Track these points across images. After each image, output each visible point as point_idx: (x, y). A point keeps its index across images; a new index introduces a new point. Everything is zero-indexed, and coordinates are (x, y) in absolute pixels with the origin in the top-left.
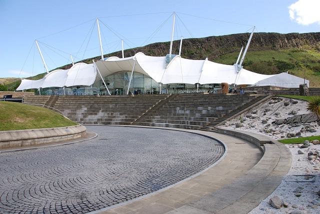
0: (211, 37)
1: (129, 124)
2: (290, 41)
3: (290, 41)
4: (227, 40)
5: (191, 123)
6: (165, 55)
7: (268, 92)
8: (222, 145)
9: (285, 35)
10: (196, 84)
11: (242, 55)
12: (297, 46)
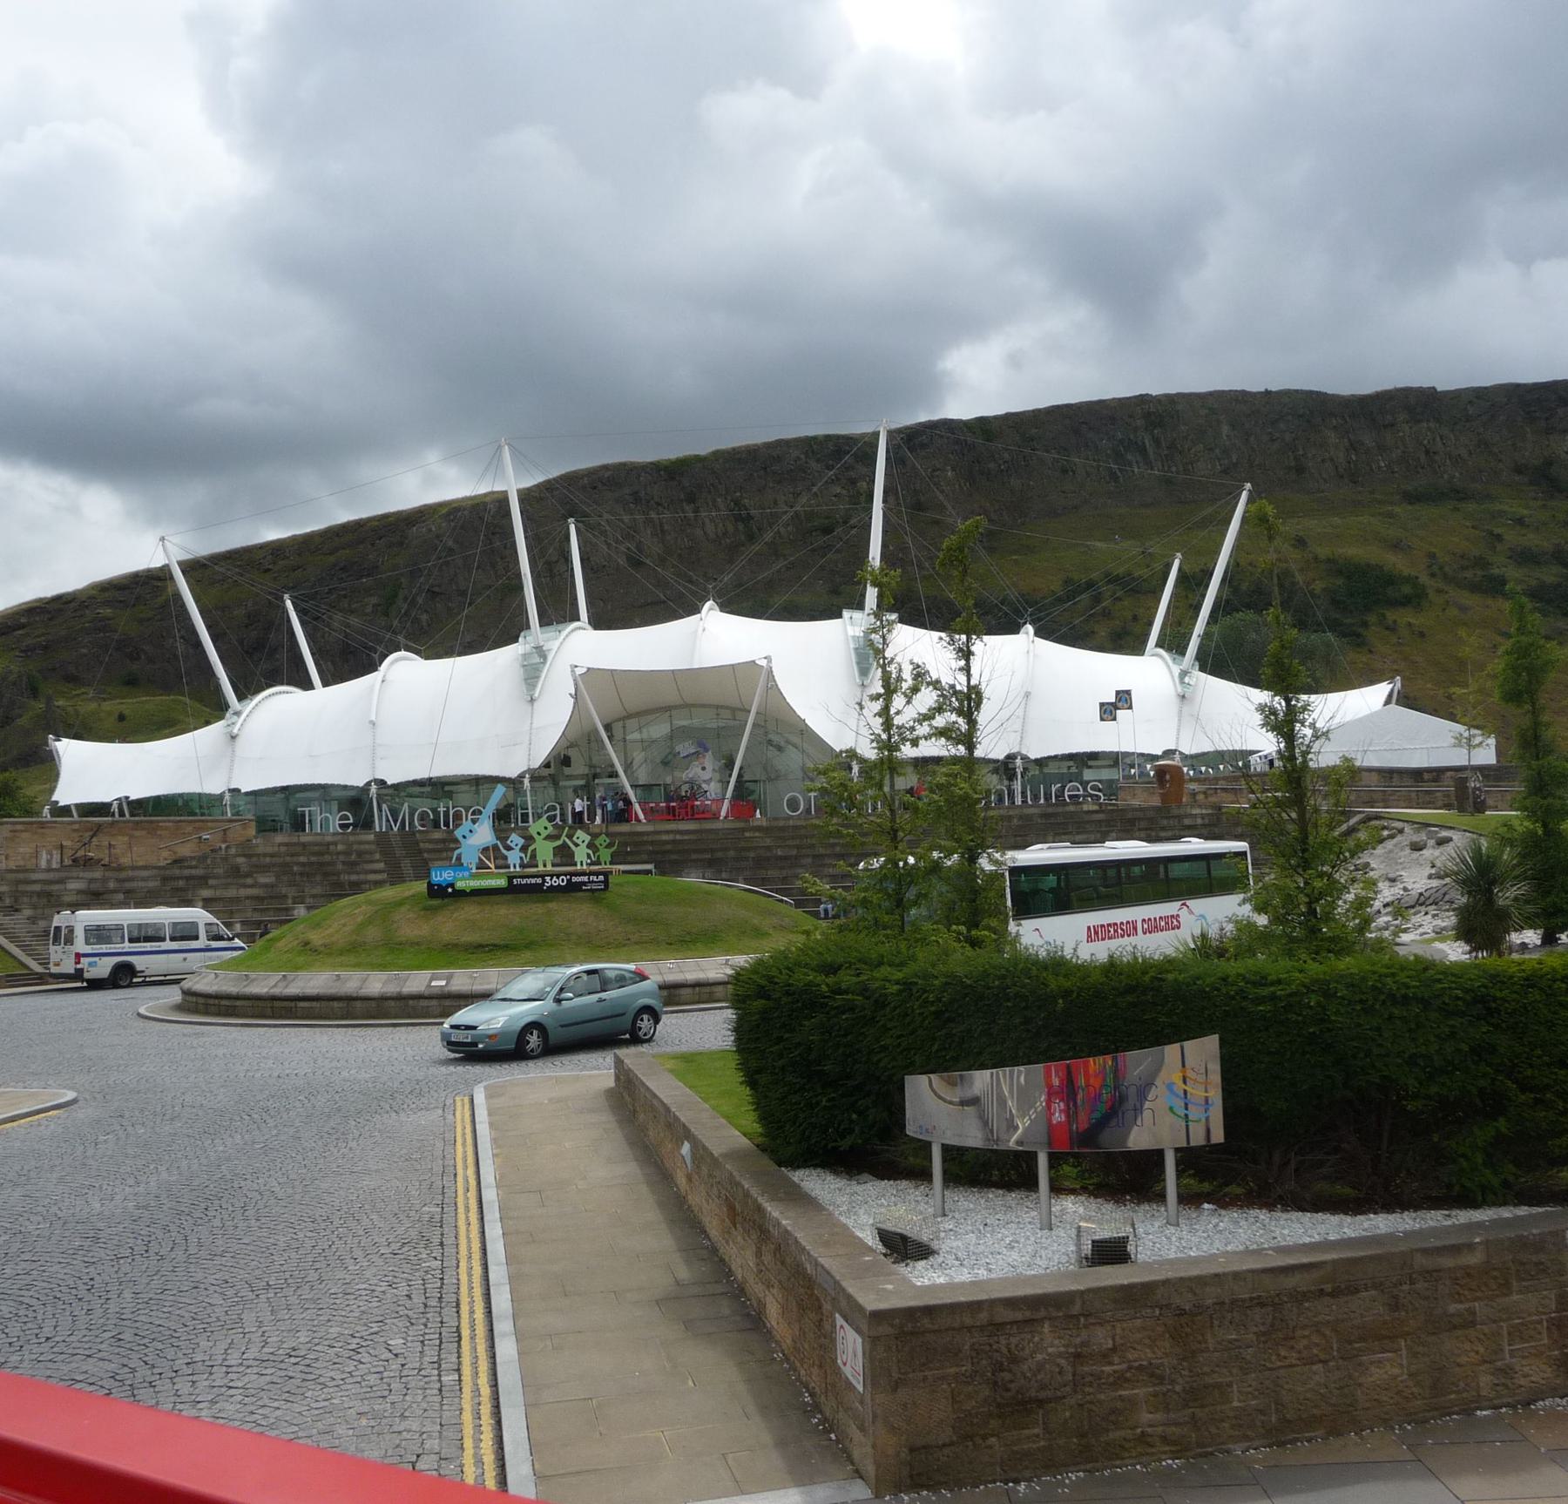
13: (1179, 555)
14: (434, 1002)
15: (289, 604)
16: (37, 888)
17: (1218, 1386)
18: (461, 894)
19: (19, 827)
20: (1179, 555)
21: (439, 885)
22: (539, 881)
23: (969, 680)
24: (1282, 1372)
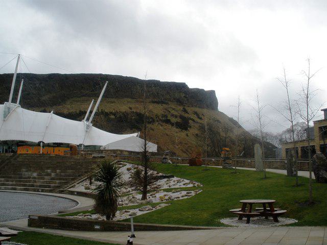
1: (38, 191)
5: (40, 186)
6: (17, 74)
7: (116, 156)
8: (75, 201)
10: (41, 142)
11: (94, 106)
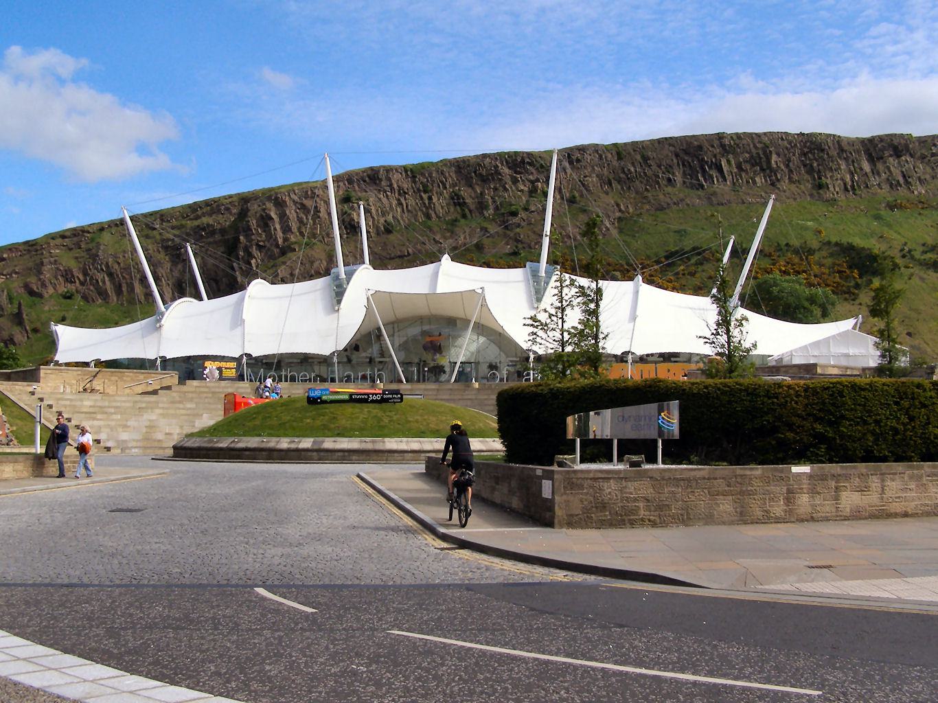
0: (582, 149)
2: (880, 166)
3: (880, 166)
4: (645, 159)
9: (863, 142)
12: (907, 183)
13: (733, 237)
14: (315, 454)
15: (189, 248)
16: (68, 403)
17: (668, 505)
18: (325, 402)
19: (49, 371)
20: (733, 237)
21: (313, 398)
22: (366, 397)
23: (597, 286)
24: (690, 503)
